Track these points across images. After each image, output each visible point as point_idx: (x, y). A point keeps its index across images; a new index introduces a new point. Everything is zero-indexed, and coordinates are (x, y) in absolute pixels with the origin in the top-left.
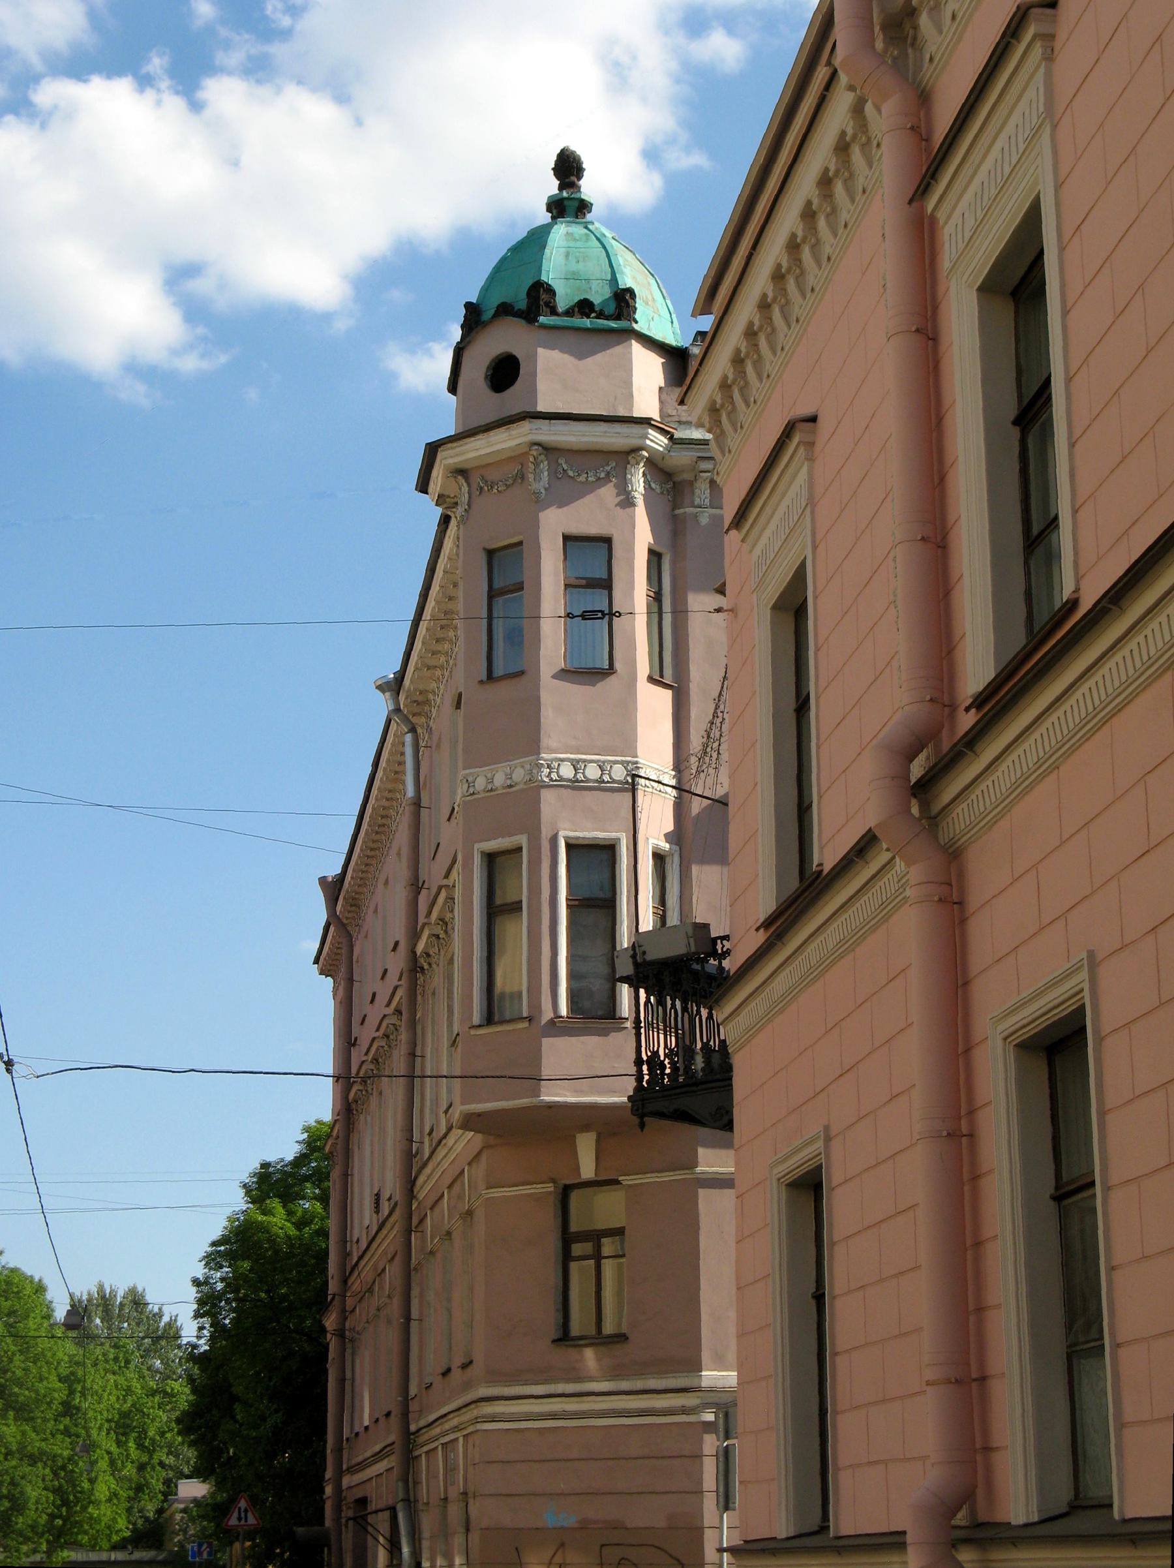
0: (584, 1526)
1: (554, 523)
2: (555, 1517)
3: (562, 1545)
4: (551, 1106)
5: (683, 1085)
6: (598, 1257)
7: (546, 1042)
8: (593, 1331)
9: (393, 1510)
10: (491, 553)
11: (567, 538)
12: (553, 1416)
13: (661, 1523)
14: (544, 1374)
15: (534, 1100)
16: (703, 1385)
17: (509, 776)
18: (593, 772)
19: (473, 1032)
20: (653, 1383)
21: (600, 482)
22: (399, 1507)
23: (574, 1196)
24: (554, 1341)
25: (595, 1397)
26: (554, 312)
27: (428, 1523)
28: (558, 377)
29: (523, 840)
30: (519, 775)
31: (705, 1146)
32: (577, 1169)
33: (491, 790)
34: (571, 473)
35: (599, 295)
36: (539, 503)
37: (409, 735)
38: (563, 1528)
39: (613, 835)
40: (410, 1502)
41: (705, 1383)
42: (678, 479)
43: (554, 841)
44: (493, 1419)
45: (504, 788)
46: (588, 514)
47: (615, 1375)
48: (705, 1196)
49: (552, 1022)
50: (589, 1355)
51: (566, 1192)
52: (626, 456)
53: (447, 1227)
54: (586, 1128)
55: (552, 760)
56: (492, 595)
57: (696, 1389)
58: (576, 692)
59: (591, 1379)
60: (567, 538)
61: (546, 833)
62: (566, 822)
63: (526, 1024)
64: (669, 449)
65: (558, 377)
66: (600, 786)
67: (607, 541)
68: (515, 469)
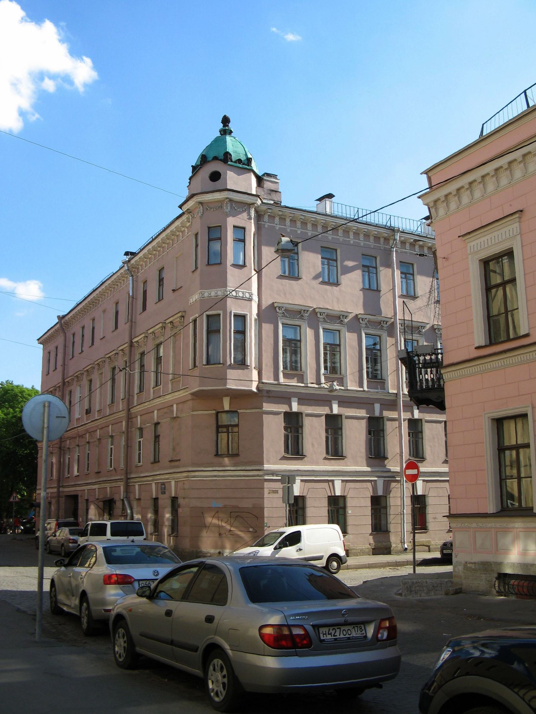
0: (225, 507)
1: (231, 221)
2: (215, 504)
4: (231, 389)
5: (436, 388)
6: (228, 432)
8: (226, 453)
9: (123, 500)
10: (209, 228)
11: (234, 227)
12: (215, 476)
15: (224, 387)
18: (241, 294)
19: (204, 366)
20: (248, 468)
22: (125, 499)
23: (219, 415)
25: (229, 471)
26: (232, 161)
27: (135, 504)
28: (233, 180)
29: (221, 312)
30: (220, 293)
35: (243, 158)
36: (228, 215)
39: (246, 313)
40: (127, 498)
42: (260, 213)
43: (231, 313)
44: (194, 477)
46: (240, 220)
47: (235, 465)
48: (265, 416)
49: (230, 365)
50: (226, 460)
51: (218, 413)
52: (250, 205)
53: (156, 421)
54: (227, 396)
56: (209, 240)
58: (236, 271)
59: (227, 466)
60: (234, 227)
61: (228, 311)
62: (234, 308)
63: (222, 365)
64: (261, 205)
65: (233, 180)
66: (242, 299)
67: (244, 228)
68: (220, 204)
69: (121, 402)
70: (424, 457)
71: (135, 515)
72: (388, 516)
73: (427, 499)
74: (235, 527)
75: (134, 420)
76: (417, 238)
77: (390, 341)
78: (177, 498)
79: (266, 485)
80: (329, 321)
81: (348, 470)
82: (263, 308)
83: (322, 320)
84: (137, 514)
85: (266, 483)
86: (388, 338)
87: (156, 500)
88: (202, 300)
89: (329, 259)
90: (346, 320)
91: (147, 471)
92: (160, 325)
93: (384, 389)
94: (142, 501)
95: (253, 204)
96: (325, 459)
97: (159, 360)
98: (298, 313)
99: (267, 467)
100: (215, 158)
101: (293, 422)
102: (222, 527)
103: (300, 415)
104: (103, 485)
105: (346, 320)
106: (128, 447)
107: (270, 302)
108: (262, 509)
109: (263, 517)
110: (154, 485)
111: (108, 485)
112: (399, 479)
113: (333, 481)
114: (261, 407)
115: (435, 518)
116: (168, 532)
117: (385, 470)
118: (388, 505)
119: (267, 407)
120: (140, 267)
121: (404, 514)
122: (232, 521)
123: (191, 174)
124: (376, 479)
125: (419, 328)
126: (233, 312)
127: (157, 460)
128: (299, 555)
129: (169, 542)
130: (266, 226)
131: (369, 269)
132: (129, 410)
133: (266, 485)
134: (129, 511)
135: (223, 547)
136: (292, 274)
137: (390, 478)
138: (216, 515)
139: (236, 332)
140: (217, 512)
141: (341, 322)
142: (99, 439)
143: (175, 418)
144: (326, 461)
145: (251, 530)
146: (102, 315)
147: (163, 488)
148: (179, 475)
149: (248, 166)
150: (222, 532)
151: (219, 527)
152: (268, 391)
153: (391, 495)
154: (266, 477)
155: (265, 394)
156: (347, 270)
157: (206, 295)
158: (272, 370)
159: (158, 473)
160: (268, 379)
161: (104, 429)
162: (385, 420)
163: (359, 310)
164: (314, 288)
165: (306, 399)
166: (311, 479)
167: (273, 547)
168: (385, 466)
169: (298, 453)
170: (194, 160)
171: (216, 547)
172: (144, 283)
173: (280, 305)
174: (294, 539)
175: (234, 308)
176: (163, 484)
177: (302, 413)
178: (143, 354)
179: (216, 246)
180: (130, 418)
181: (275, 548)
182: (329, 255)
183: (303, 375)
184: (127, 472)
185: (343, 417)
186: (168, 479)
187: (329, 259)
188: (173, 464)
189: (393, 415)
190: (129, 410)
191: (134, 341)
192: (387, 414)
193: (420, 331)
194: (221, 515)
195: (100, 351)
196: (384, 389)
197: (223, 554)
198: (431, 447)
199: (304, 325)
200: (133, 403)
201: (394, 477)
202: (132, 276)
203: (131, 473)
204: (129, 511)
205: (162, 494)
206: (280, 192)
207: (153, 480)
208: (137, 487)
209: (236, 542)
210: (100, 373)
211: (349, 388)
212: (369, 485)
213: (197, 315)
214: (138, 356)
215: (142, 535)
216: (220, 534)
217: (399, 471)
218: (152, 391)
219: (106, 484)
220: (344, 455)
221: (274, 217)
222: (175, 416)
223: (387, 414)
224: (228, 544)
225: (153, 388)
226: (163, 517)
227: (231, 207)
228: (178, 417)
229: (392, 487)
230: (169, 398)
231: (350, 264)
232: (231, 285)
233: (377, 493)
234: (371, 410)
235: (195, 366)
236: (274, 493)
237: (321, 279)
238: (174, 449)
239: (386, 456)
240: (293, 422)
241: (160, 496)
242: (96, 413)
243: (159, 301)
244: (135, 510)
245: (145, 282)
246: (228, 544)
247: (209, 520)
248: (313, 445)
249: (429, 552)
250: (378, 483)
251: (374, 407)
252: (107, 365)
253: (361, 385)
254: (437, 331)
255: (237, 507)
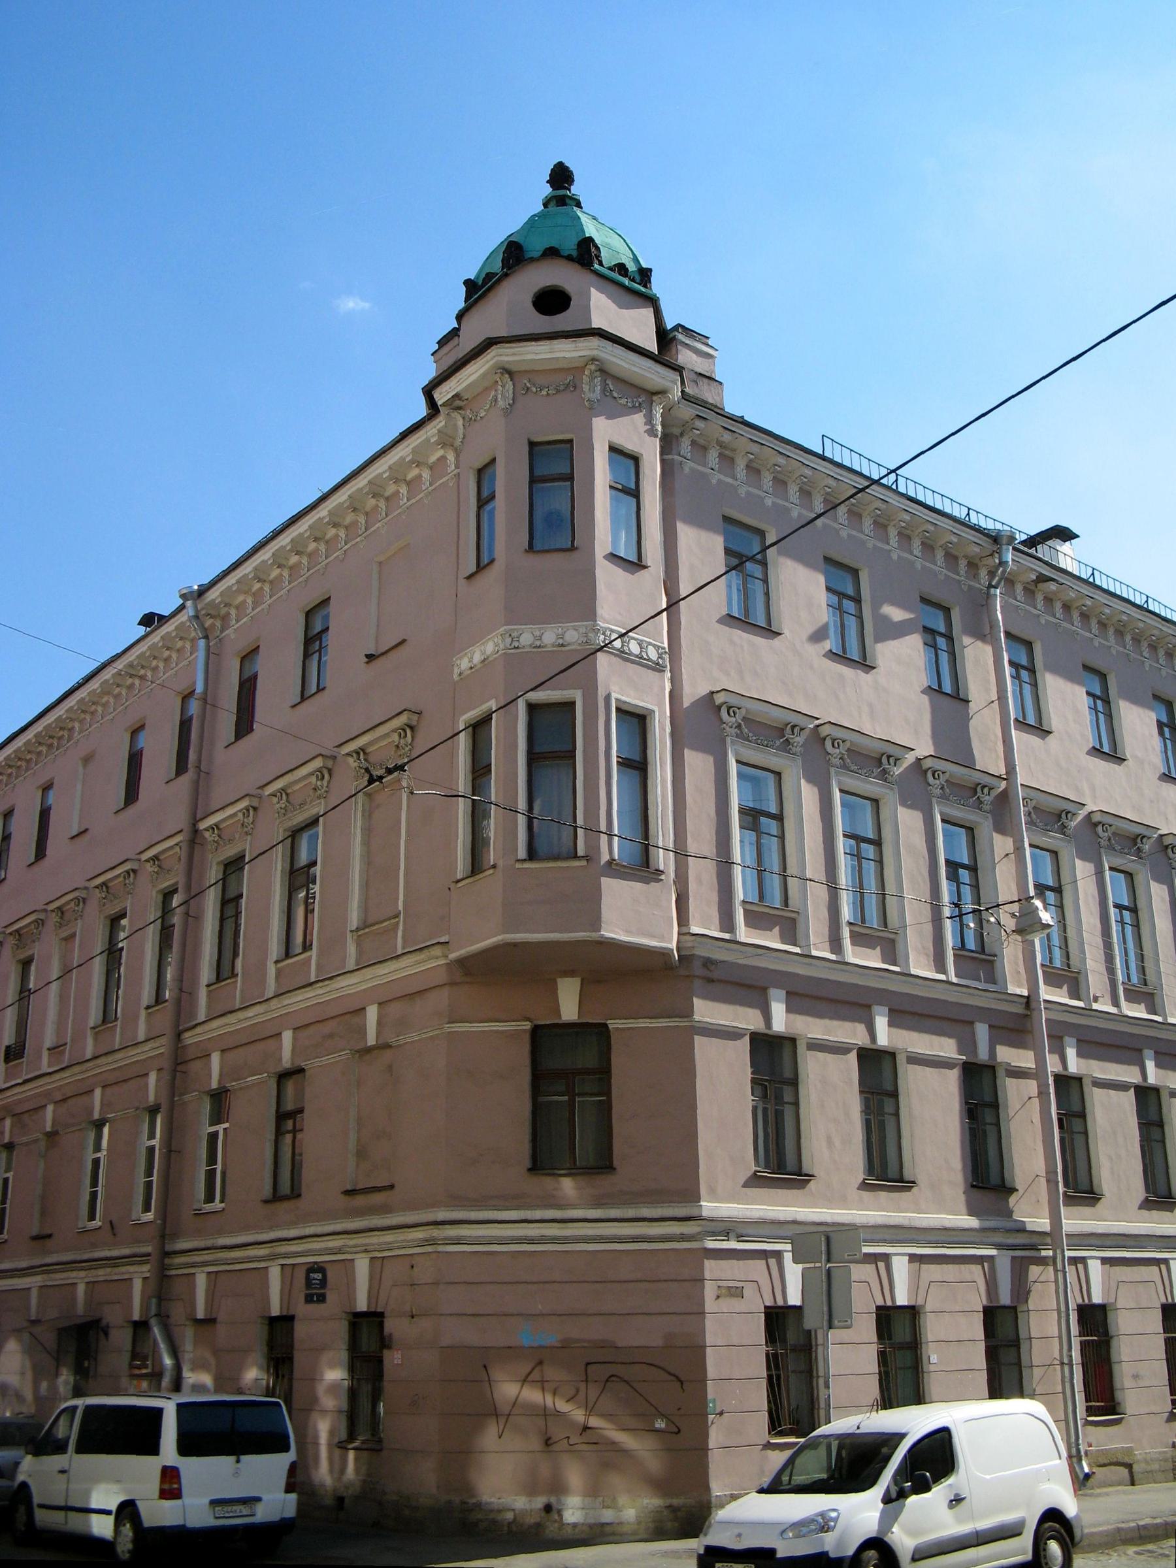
0: (565, 1345)
1: (606, 431)
2: (526, 1336)
3: (541, 1363)
7: (606, 882)
10: (532, 445)
13: (659, 1342)
14: (517, 1200)
15: (594, 936)
16: (704, 1214)
17: (483, 653)
19: (518, 865)
20: (646, 1212)
21: (636, 409)
24: (529, 1170)
25: (573, 1221)
27: (187, 1338)
31: (698, 997)
32: (557, 1012)
33: (562, 645)
34: (615, 395)
36: (593, 409)
37: (203, 641)
38: (541, 1347)
41: (705, 1213)
43: (608, 698)
44: (458, 1241)
45: (553, 646)
47: (598, 1203)
49: (611, 861)
54: (571, 973)
55: (606, 629)
56: (533, 480)
57: (700, 1218)
61: (601, 693)
62: (618, 684)
68: (567, 379)
69: (143, 1013)
70: (1096, 1189)
71: (186, 1374)
72: (1025, 1372)
73: (1111, 1316)
74: (602, 1415)
75: (196, 1066)
76: (1047, 571)
77: (1002, 844)
78: (381, 1315)
79: (711, 1268)
80: (855, 768)
81: (924, 1224)
82: (686, 703)
83: (837, 761)
84: (192, 1370)
85: (709, 1264)
86: (995, 835)
87: (287, 1320)
88: (514, 658)
89: (841, 595)
90: (897, 771)
91: (246, 1228)
92: (318, 763)
93: (994, 981)
94: (221, 1330)
95: (662, 392)
96: (864, 1186)
97: (299, 877)
98: (778, 732)
99: (709, 1207)
100: (551, 253)
101: (773, 1060)
102: (558, 1414)
103: (787, 1044)
104: (59, 1278)
105: (897, 771)
106: (170, 1151)
107: (703, 690)
108: (697, 1351)
109: (701, 1379)
110: (275, 1273)
111: (80, 1280)
112: (1050, 1253)
113: (886, 1258)
114: (688, 1013)
115: (1136, 1377)
116: (332, 1433)
117: (1009, 1225)
118: (1023, 1334)
119: (706, 1011)
120: (233, 612)
121: (1071, 1365)
122: (593, 1392)
123: (461, 305)
124: (993, 1252)
125: (1060, 816)
126: (614, 695)
127: (285, 1188)
128: (959, 1520)
129: (339, 1469)
130: (687, 470)
131: (941, 641)
132: (178, 1035)
133: (711, 1268)
134: (168, 1361)
135: (558, 1487)
136: (754, 619)
137: (1027, 1250)
138: (536, 1375)
139: (624, 763)
140: (537, 1363)
141: (884, 775)
142: (52, 1135)
143: (369, 1050)
144: (866, 1195)
145: (660, 1424)
146: (81, 769)
147: (316, 1282)
148: (389, 1237)
149: (645, 286)
150: (557, 1433)
151: (546, 1414)
152: (708, 963)
153: (1031, 1305)
154: (711, 1244)
155: (698, 970)
156: (896, 631)
157: (526, 639)
158: (715, 897)
159: (293, 1233)
160: (705, 924)
161: (71, 1102)
162: (1000, 1073)
163: (924, 747)
164: (811, 667)
165: (811, 996)
166: (825, 1246)
167: (875, 1494)
168: (1009, 1213)
169: (780, 1167)
170: (475, 255)
171: (531, 1490)
172: (243, 659)
173: (733, 700)
174: (934, 1458)
175: (618, 684)
176: (319, 1268)
177: (793, 1041)
178: (234, 866)
179: (555, 499)
180: (179, 1063)
181: (887, 1500)
182: (845, 583)
183: (794, 920)
184: (166, 1231)
185: (901, 1059)
186: (340, 1251)
187: (841, 595)
188: (360, 1201)
189: (1024, 1059)
190: (178, 1035)
191: (202, 825)
192: (1007, 1055)
193: (1064, 826)
194: (552, 1373)
195: (68, 868)
196: (994, 981)
197: (560, 1512)
198: (1110, 1158)
199: (793, 772)
200: (193, 1014)
201: (1033, 1247)
202: (206, 637)
203: (175, 1236)
204: (168, 1361)
205: (309, 1299)
206: (721, 383)
207: (273, 1257)
208: (201, 1281)
209: (606, 1466)
210: (65, 935)
211: (913, 971)
212: (975, 1272)
213: (493, 705)
214: (214, 873)
215: (286, 1449)
216: (548, 1442)
217: (1047, 1228)
218: (272, 970)
219: (74, 1274)
220: (907, 1175)
221: (705, 449)
222: (371, 1040)
223: (1007, 1055)
224: (575, 1476)
225: (277, 962)
226: (313, 1379)
227: (604, 391)
228: (387, 1046)
229: (1031, 1278)
230: (349, 985)
231: (896, 614)
232: (606, 616)
233: (998, 1301)
234: (967, 1043)
235: (476, 866)
236: (732, 1295)
237: (827, 645)
238: (361, 1154)
239: (1008, 1184)
240: (773, 1060)
241: (301, 1309)
242: (45, 1054)
243: (303, 698)
244: (187, 1356)
245: (249, 656)
246: (575, 1476)
247: (508, 1389)
248: (829, 1141)
249: (1133, 1484)
250: (998, 1261)
251: (973, 1034)
252: (92, 909)
253: (941, 967)
254: (1100, 828)
255: (602, 1345)
